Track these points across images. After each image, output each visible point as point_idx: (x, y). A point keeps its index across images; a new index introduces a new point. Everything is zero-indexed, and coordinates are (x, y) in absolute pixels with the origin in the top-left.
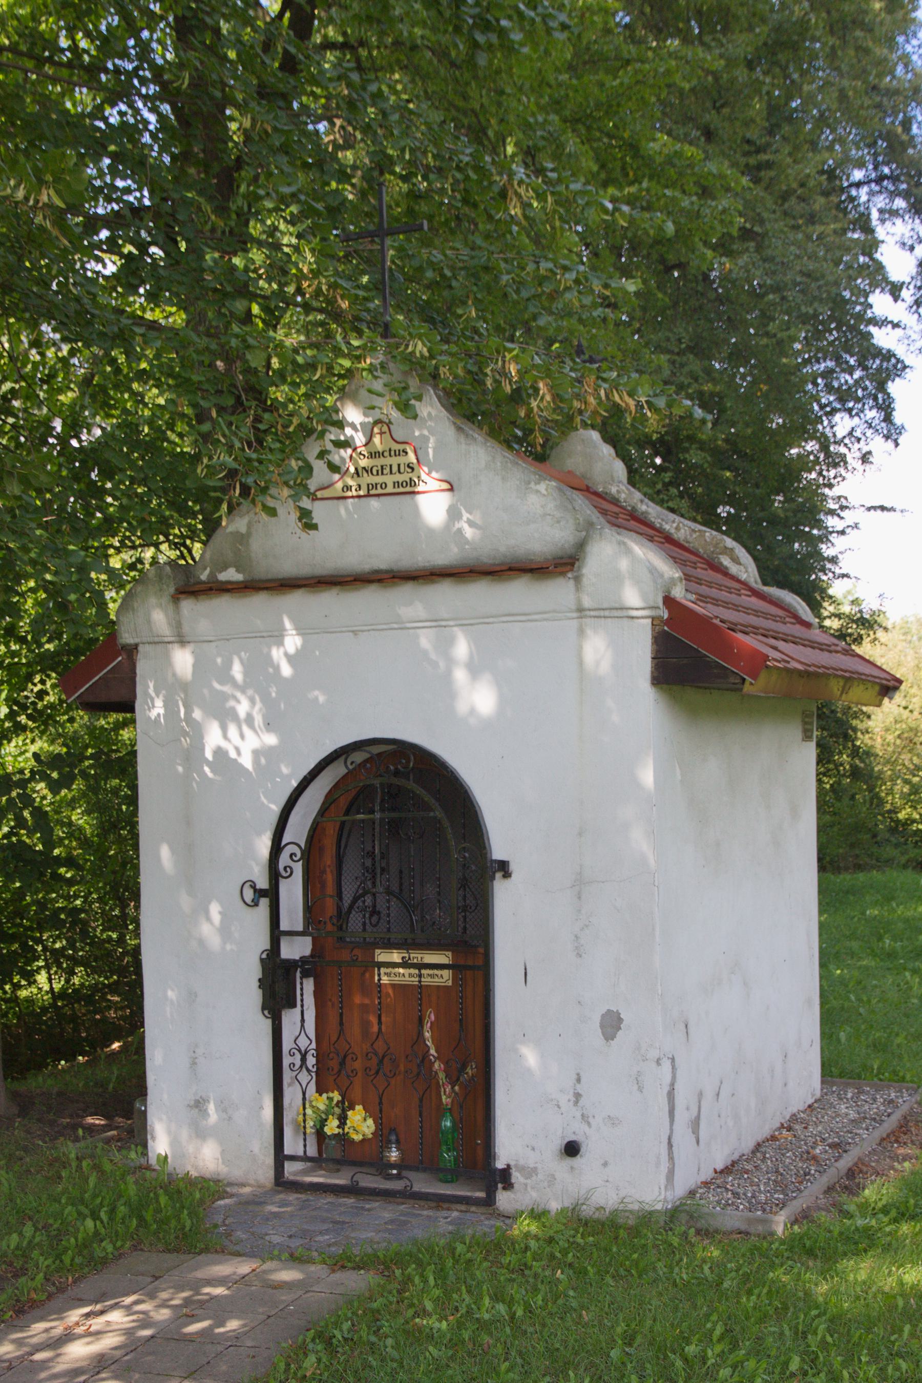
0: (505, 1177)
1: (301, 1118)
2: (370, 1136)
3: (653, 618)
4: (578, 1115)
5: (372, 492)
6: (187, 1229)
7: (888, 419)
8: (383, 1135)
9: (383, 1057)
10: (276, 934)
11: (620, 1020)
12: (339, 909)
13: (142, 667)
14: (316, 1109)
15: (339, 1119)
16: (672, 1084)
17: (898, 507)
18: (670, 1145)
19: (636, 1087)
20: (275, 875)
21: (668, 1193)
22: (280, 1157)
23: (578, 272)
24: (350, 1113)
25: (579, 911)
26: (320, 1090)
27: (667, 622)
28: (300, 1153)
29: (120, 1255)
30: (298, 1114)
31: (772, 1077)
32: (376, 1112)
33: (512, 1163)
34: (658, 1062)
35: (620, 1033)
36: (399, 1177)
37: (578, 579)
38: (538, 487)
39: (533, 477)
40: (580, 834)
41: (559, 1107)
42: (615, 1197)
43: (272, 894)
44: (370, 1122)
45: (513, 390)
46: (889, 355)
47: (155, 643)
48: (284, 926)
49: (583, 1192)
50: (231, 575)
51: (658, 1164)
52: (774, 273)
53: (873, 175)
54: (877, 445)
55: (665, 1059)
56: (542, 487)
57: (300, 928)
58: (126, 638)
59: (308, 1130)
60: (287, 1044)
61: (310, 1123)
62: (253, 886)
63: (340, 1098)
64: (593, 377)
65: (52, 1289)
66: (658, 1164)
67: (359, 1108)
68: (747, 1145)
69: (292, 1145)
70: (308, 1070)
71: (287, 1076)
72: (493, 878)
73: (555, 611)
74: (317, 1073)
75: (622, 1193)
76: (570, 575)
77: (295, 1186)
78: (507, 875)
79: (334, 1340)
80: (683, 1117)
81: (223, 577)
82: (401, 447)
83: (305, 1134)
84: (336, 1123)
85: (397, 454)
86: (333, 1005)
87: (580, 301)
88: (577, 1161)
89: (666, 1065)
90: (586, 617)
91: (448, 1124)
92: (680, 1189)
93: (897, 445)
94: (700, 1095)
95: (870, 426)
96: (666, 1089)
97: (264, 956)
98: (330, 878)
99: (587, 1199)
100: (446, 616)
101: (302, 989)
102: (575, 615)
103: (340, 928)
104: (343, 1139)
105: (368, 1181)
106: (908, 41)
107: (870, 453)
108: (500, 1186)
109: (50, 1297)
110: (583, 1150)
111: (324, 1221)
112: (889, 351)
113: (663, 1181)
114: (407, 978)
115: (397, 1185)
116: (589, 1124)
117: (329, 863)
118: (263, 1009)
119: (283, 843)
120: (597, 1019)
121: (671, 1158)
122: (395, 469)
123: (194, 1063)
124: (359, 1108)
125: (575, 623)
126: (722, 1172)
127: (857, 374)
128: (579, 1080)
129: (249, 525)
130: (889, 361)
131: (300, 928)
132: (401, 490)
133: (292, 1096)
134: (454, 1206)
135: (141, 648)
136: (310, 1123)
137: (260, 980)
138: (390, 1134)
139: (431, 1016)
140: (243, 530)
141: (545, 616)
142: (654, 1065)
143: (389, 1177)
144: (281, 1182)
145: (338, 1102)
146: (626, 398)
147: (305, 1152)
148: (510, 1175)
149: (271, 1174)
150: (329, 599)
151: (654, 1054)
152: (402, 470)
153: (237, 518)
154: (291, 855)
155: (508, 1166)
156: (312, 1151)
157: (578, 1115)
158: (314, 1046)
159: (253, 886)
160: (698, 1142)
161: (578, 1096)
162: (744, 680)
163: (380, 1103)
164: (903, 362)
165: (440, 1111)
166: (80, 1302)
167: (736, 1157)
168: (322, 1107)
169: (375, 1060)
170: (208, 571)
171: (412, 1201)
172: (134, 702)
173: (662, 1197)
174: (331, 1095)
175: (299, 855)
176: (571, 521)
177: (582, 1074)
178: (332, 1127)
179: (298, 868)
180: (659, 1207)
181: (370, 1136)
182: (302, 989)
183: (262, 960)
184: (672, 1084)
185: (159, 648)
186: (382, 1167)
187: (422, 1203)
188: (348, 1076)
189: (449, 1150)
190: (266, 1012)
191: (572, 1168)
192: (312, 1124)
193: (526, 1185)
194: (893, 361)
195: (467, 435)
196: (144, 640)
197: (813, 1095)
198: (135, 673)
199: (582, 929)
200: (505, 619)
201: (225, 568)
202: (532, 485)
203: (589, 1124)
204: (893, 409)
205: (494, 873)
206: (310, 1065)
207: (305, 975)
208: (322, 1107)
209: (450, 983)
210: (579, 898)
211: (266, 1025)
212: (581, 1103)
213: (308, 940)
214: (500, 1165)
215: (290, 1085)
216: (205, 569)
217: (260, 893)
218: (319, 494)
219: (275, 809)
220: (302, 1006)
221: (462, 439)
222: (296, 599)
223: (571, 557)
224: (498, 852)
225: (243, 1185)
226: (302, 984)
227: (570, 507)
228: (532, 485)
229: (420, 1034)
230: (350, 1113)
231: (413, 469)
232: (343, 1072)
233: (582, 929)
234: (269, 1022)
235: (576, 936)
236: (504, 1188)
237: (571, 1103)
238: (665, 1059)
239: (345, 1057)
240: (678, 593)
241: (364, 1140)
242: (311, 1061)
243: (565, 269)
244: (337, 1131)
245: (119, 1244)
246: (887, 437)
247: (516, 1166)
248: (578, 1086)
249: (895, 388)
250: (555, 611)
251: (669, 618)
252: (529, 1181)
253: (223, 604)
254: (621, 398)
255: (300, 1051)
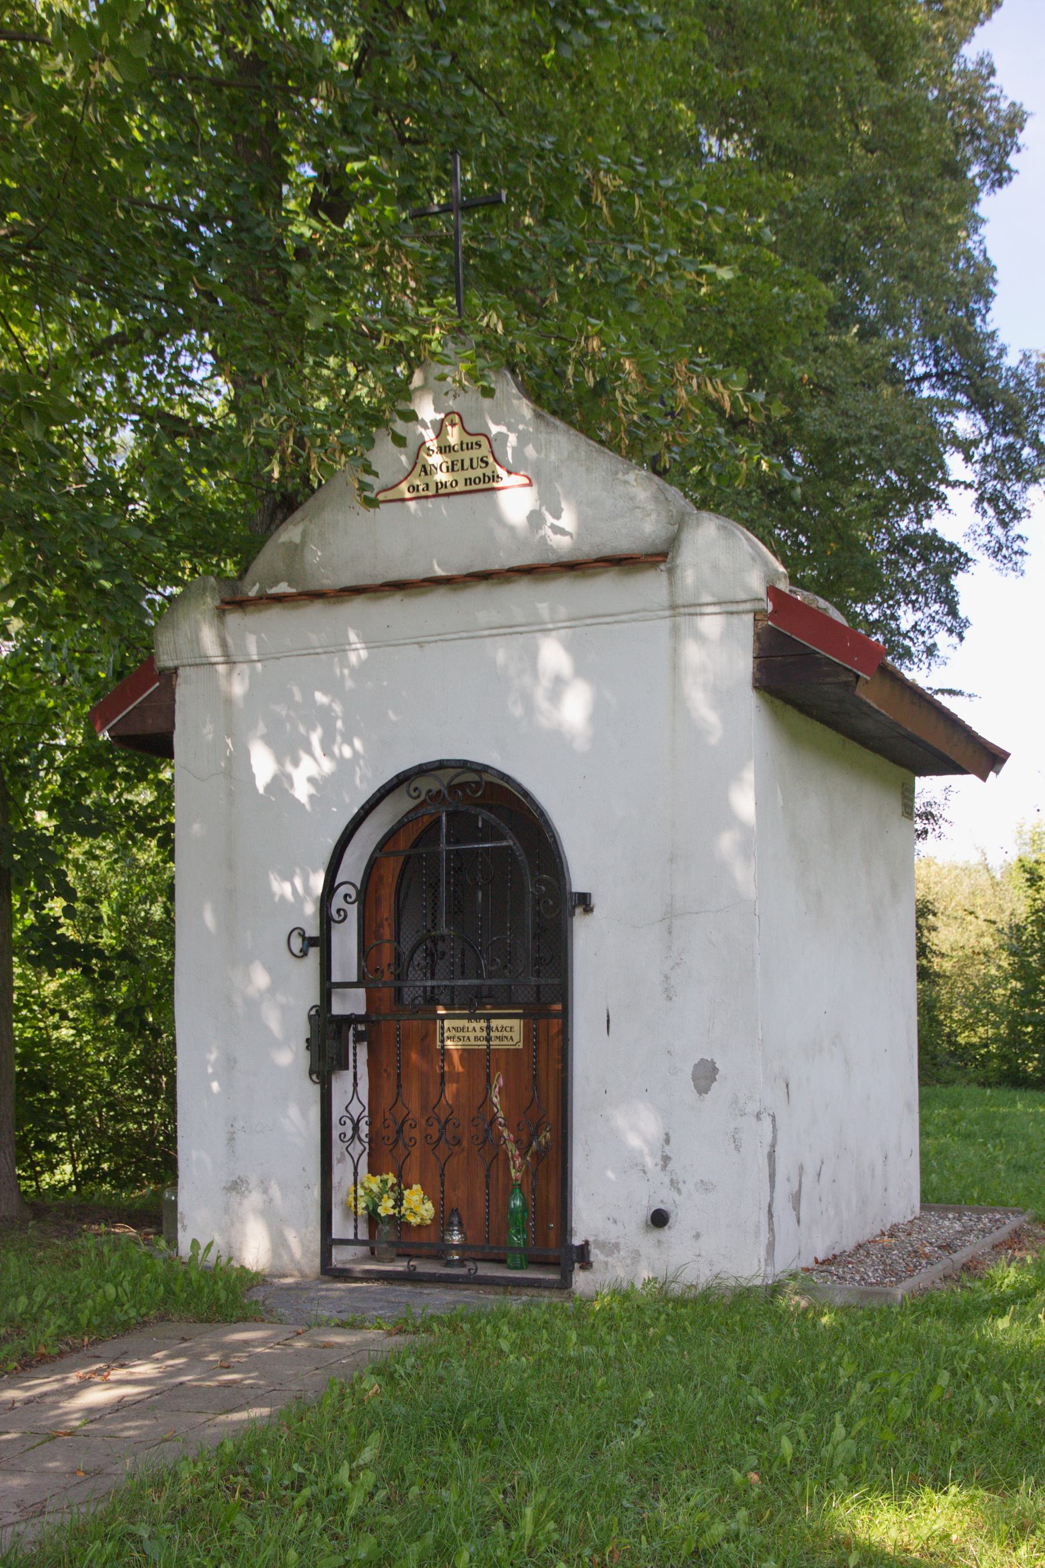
0: (582, 1256)
1: (351, 1198)
2: (429, 1222)
3: (755, 613)
4: (667, 1181)
5: (440, 492)
6: (222, 1301)
7: (953, 612)
8: (444, 1219)
9: (447, 1121)
10: (327, 987)
11: (715, 1070)
12: (398, 956)
13: (183, 692)
14: (369, 1191)
15: (396, 1200)
16: (773, 1146)
17: (967, 691)
18: (771, 1215)
19: (733, 1146)
20: (326, 920)
21: (769, 1269)
22: (328, 1242)
23: (670, 256)
24: (406, 1193)
25: (669, 948)
26: (373, 1170)
27: (771, 617)
28: (351, 1236)
29: (144, 1322)
30: (348, 1195)
31: (873, 1176)
32: (437, 1195)
33: (591, 1239)
34: (758, 1116)
35: (715, 1085)
36: (461, 1263)
37: (671, 572)
38: (626, 477)
39: (620, 466)
40: (671, 860)
41: (644, 1172)
42: (708, 1274)
43: (322, 943)
44: (429, 1205)
45: (596, 383)
46: (952, 548)
47: (197, 665)
48: (336, 978)
49: (671, 1270)
50: (283, 588)
51: (757, 1234)
52: (847, 426)
53: (934, 371)
54: (942, 639)
55: (765, 1114)
56: (631, 477)
57: (354, 978)
58: (165, 660)
59: (360, 1211)
60: (337, 1111)
61: (362, 1205)
62: (302, 935)
63: (395, 1181)
64: (685, 360)
65: (64, 1347)
66: (757, 1234)
67: (417, 1187)
68: (849, 1245)
69: (341, 1228)
70: (360, 1140)
71: (336, 1154)
72: (573, 914)
73: (645, 610)
74: (369, 1143)
75: (715, 1271)
76: (662, 567)
77: (343, 1275)
78: (588, 909)
79: (396, 1375)
80: (783, 1190)
81: (274, 591)
82: (474, 439)
83: (356, 1213)
84: (391, 1203)
85: (470, 447)
86: (389, 1075)
87: (673, 286)
88: (665, 1234)
89: (767, 1121)
90: (680, 614)
91: (518, 1203)
92: (786, 1260)
93: (961, 639)
94: (801, 1168)
95: (933, 620)
96: (766, 1149)
97: (313, 1012)
98: (387, 932)
99: (676, 1277)
100: (523, 620)
101: (355, 1055)
102: (667, 613)
103: (398, 977)
104: (397, 1221)
105: (424, 1267)
106: (968, 236)
107: (934, 645)
108: (577, 1265)
109: (61, 1354)
110: (671, 1221)
111: (376, 1300)
112: (951, 545)
113: (763, 1253)
114: (473, 1042)
115: (462, 1271)
116: (679, 1191)
117: (386, 915)
118: (310, 1074)
119: (336, 884)
120: (689, 1070)
121: (771, 1230)
122: (467, 464)
123: (231, 1139)
124: (417, 1187)
125: (667, 623)
126: (823, 1263)
127: (920, 567)
128: (667, 1141)
129: (304, 534)
130: (951, 554)
131: (354, 978)
132: (474, 487)
133: (342, 1174)
134: (524, 1291)
135: (180, 672)
136: (362, 1205)
137: (308, 1040)
138: (452, 1214)
139: (499, 1081)
140: (297, 539)
141: (634, 616)
142: (754, 1119)
143: (449, 1264)
144: (329, 1271)
145: (393, 1185)
146: (721, 388)
147: (356, 1234)
148: (588, 1252)
149: (317, 1261)
150: (392, 607)
151: (753, 1107)
152: (475, 465)
153: (291, 527)
154: (346, 896)
155: (587, 1243)
156: (363, 1234)
157: (667, 1181)
158: (366, 1113)
159: (302, 935)
160: (799, 1222)
161: (666, 1159)
162: (858, 677)
163: (442, 1175)
164: (966, 555)
165: (509, 1188)
166: (98, 1358)
167: (837, 1252)
168: (375, 1188)
169: (436, 1126)
170: (257, 587)
171: (476, 1287)
172: (172, 733)
173: (762, 1272)
174: (385, 1177)
175: (354, 897)
176: (664, 514)
177: (671, 1134)
178: (386, 1207)
179: (353, 911)
180: (758, 1282)
181: (429, 1222)
182: (355, 1055)
183: (310, 1017)
184: (773, 1146)
185: (201, 670)
186: (439, 1252)
187: (488, 1289)
188: (405, 1145)
189: (518, 1232)
190: (314, 1077)
191: (659, 1242)
192: (364, 1205)
193: (606, 1263)
194: (956, 555)
195: (548, 424)
196: (185, 662)
197: (913, 1212)
198: (174, 700)
199: (672, 968)
200: (589, 621)
201: (276, 583)
202: (620, 476)
203: (679, 1191)
204: (957, 603)
205: (574, 907)
206: (363, 1136)
207: (359, 1038)
208: (375, 1188)
209: (521, 1046)
210: (670, 933)
211: (314, 1091)
212: (669, 1168)
213: (361, 992)
214: (577, 1241)
215: (339, 1161)
216: (254, 585)
217: (310, 942)
218: (381, 497)
219: (331, 842)
220: (355, 1067)
221: (542, 428)
222: (356, 607)
223: (661, 547)
224: (578, 883)
225: (285, 1276)
226: (355, 1048)
227: (662, 498)
228: (620, 476)
229: (487, 1098)
230: (406, 1193)
231: (487, 463)
232: (400, 1143)
233: (672, 968)
234: (317, 1089)
235: (666, 977)
236: (581, 1268)
237: (659, 1167)
238: (765, 1114)
239: (403, 1122)
240: (784, 586)
241: (419, 1226)
242: (364, 1129)
243: (655, 252)
244: (391, 1212)
245: (143, 1310)
246: (950, 631)
247: (595, 1241)
248: (667, 1148)
249: (958, 581)
250: (645, 610)
251: (774, 611)
252: (609, 1259)
253: (274, 615)
254: (715, 390)
255: (352, 1120)
